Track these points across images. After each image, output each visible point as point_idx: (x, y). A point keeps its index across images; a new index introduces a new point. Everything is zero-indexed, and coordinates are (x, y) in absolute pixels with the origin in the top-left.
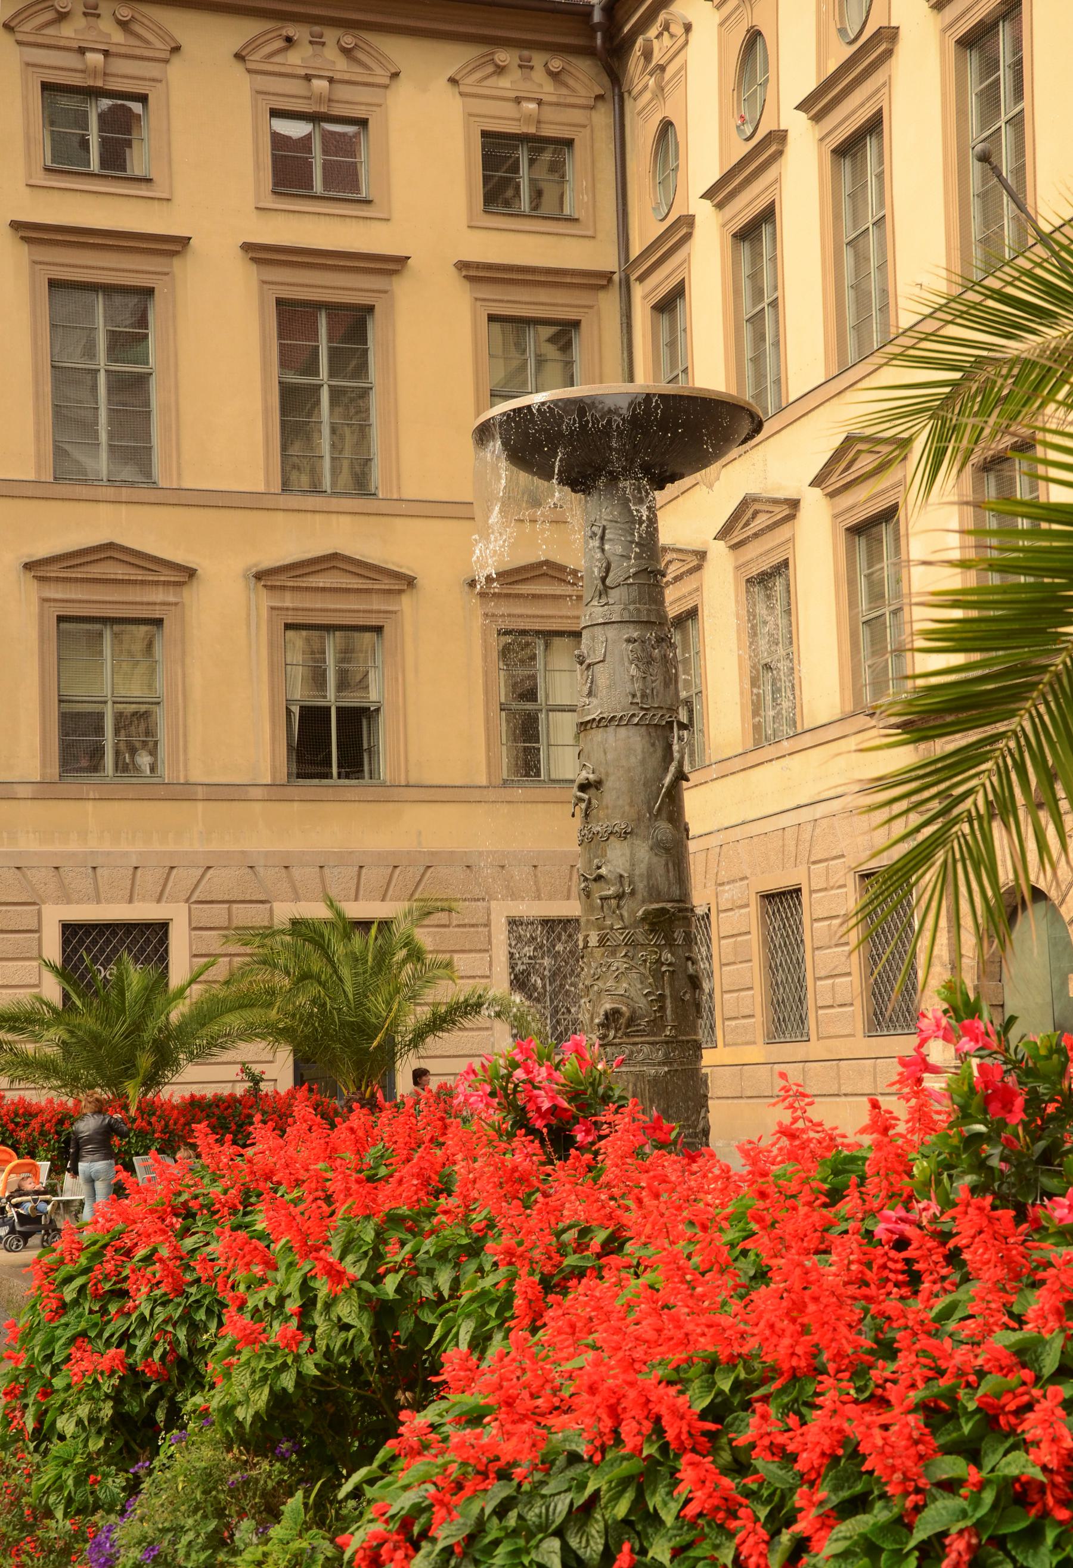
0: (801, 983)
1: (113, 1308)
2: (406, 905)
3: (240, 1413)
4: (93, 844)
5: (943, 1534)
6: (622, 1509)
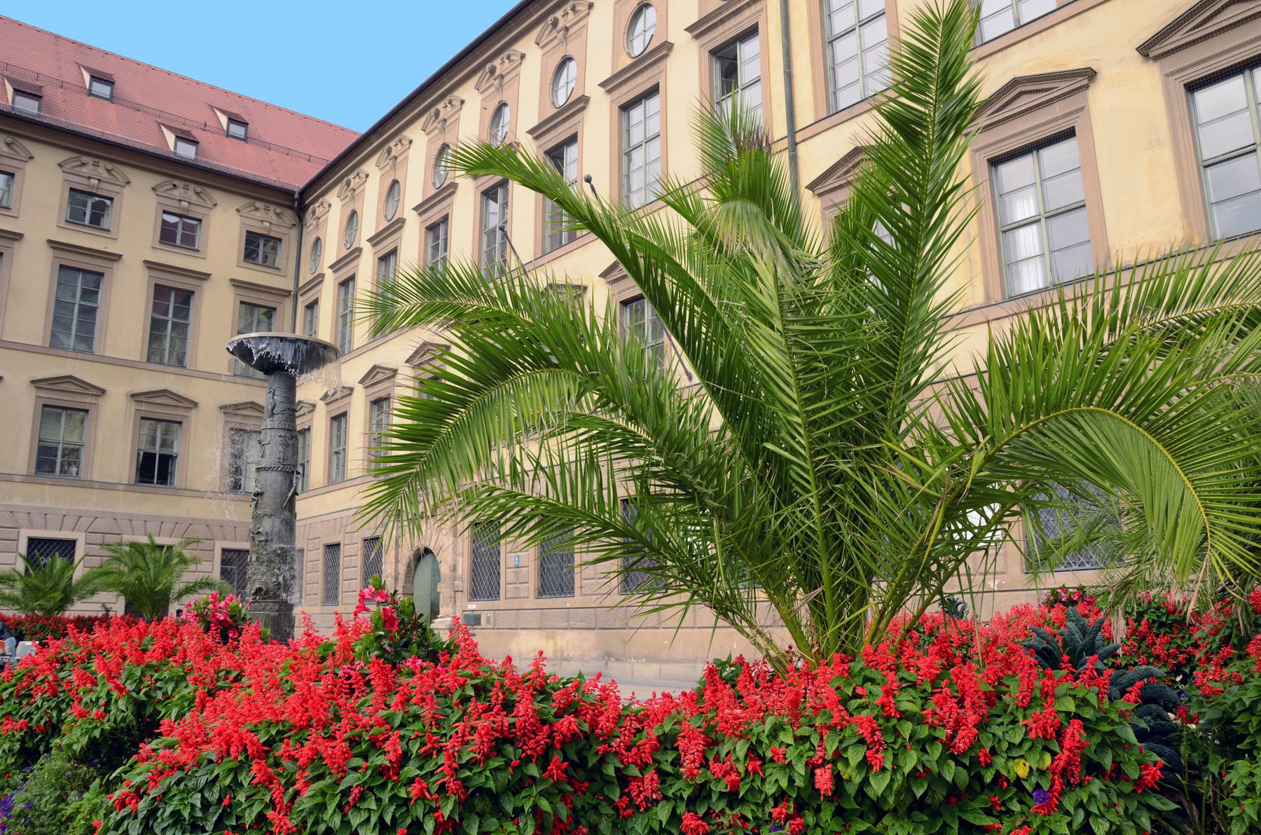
0: (337, 581)
1: (24, 702)
2: (180, 540)
3: (75, 747)
4: (46, 504)
5: (351, 787)
6: (227, 782)
